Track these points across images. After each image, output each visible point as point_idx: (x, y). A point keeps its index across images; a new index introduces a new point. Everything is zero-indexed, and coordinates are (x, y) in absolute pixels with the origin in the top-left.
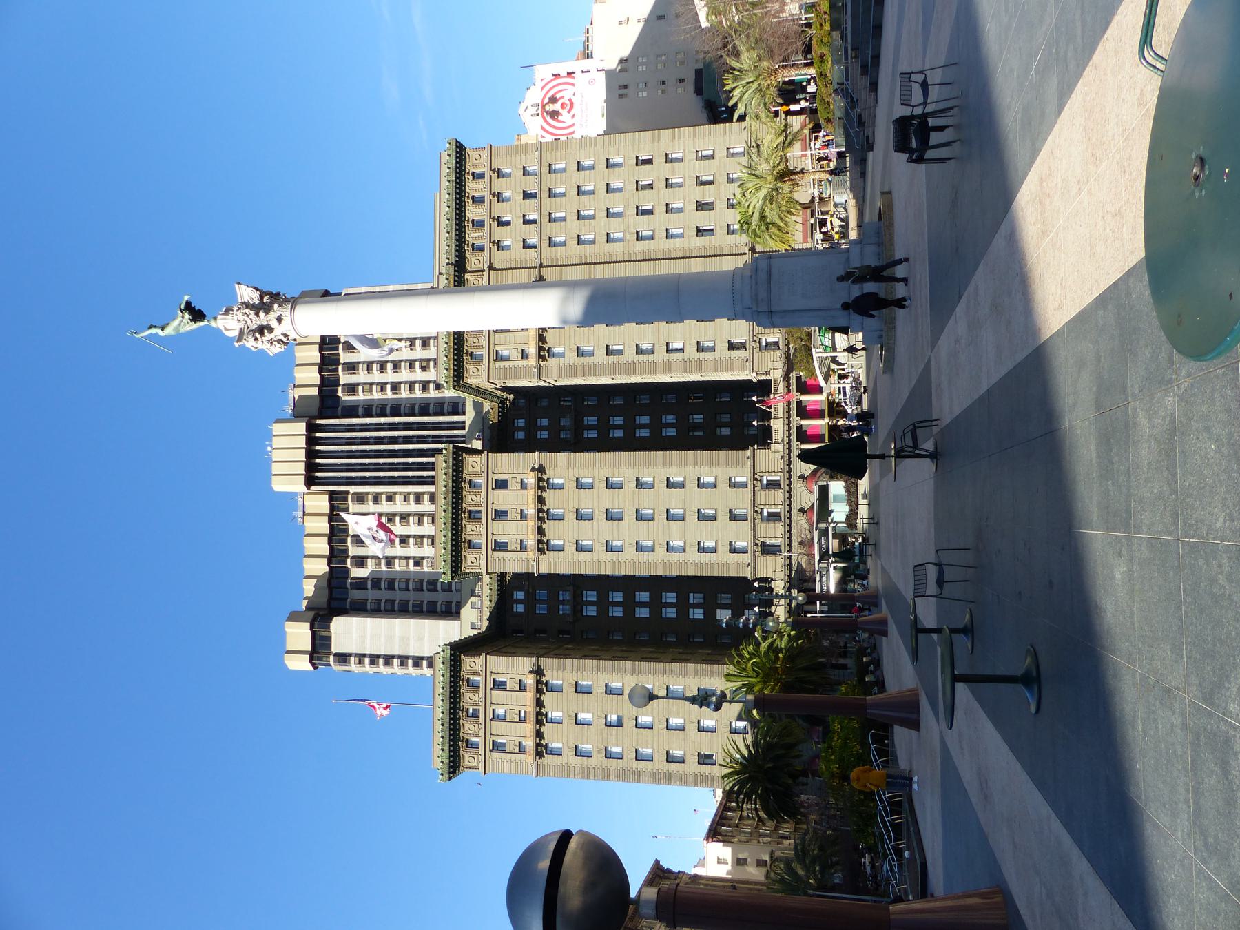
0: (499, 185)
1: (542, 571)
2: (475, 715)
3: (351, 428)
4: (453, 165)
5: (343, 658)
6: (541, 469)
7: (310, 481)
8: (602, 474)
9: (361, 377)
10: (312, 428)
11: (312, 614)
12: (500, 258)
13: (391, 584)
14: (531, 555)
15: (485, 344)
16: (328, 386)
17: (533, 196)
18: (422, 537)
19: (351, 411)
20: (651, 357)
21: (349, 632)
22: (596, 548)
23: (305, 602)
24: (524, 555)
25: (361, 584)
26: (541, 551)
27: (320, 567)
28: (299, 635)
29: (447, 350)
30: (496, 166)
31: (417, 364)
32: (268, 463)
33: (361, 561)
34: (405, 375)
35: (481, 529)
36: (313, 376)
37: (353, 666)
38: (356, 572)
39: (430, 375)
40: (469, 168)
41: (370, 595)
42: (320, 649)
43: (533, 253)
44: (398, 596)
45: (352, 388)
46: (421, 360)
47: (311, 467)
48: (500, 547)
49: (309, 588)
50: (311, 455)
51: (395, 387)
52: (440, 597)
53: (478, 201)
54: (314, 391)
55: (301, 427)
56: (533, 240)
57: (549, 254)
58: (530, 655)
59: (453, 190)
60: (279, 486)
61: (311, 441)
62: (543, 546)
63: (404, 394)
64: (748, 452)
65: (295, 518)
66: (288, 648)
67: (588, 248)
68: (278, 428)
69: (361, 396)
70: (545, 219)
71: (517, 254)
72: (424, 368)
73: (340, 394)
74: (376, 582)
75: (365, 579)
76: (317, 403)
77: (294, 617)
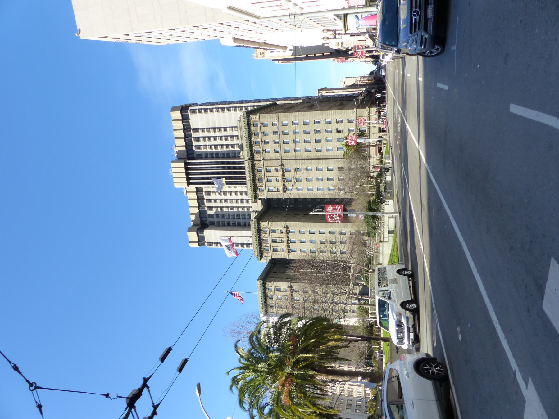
0: (264, 129)
1: (290, 258)
2: (272, 298)
3: (201, 164)
4: (246, 123)
5: (210, 244)
6: (287, 227)
7: (189, 184)
8: (308, 229)
9: (201, 143)
10: (186, 164)
11: (196, 228)
12: (267, 156)
13: (223, 216)
14: (286, 253)
15: (264, 186)
16: (189, 146)
17: (277, 132)
18: (232, 200)
19: (199, 156)
20: (322, 192)
21: (210, 235)
22: (290, 142)
23: (192, 223)
24: (283, 253)
25: (212, 216)
26: (289, 252)
27: (196, 210)
28: (193, 236)
29: (251, 189)
30: (262, 122)
31: (223, 138)
32: (172, 178)
33: (210, 208)
34: (218, 142)
35: (268, 245)
36: (182, 142)
37: (214, 246)
38: (210, 212)
39: (244, 197)
40: (252, 122)
41: (216, 220)
42: (201, 241)
43: (278, 154)
44: (226, 220)
45: (199, 147)
46: (225, 136)
47: (188, 179)
48: (275, 250)
49: (193, 218)
50: (187, 174)
51: (216, 146)
52: (242, 221)
53: (257, 135)
54: (184, 148)
55: (182, 165)
56: (278, 149)
57: (285, 155)
58: (288, 282)
59: (247, 132)
60: (177, 186)
61: (187, 169)
62: (289, 251)
63: (219, 149)
64: (354, 110)
65: (183, 193)
66: (190, 240)
67: (298, 154)
68: (173, 165)
69: (203, 150)
70: (280, 124)
71: (272, 155)
72: (226, 139)
73: (194, 149)
74: (217, 215)
75: (213, 214)
76: (186, 153)
77: (190, 230)
